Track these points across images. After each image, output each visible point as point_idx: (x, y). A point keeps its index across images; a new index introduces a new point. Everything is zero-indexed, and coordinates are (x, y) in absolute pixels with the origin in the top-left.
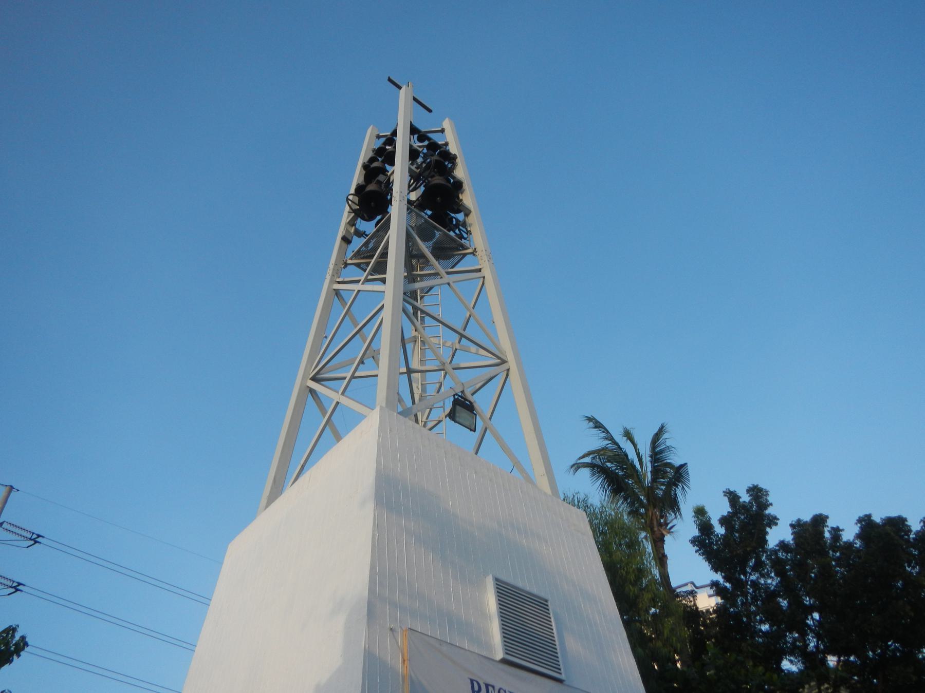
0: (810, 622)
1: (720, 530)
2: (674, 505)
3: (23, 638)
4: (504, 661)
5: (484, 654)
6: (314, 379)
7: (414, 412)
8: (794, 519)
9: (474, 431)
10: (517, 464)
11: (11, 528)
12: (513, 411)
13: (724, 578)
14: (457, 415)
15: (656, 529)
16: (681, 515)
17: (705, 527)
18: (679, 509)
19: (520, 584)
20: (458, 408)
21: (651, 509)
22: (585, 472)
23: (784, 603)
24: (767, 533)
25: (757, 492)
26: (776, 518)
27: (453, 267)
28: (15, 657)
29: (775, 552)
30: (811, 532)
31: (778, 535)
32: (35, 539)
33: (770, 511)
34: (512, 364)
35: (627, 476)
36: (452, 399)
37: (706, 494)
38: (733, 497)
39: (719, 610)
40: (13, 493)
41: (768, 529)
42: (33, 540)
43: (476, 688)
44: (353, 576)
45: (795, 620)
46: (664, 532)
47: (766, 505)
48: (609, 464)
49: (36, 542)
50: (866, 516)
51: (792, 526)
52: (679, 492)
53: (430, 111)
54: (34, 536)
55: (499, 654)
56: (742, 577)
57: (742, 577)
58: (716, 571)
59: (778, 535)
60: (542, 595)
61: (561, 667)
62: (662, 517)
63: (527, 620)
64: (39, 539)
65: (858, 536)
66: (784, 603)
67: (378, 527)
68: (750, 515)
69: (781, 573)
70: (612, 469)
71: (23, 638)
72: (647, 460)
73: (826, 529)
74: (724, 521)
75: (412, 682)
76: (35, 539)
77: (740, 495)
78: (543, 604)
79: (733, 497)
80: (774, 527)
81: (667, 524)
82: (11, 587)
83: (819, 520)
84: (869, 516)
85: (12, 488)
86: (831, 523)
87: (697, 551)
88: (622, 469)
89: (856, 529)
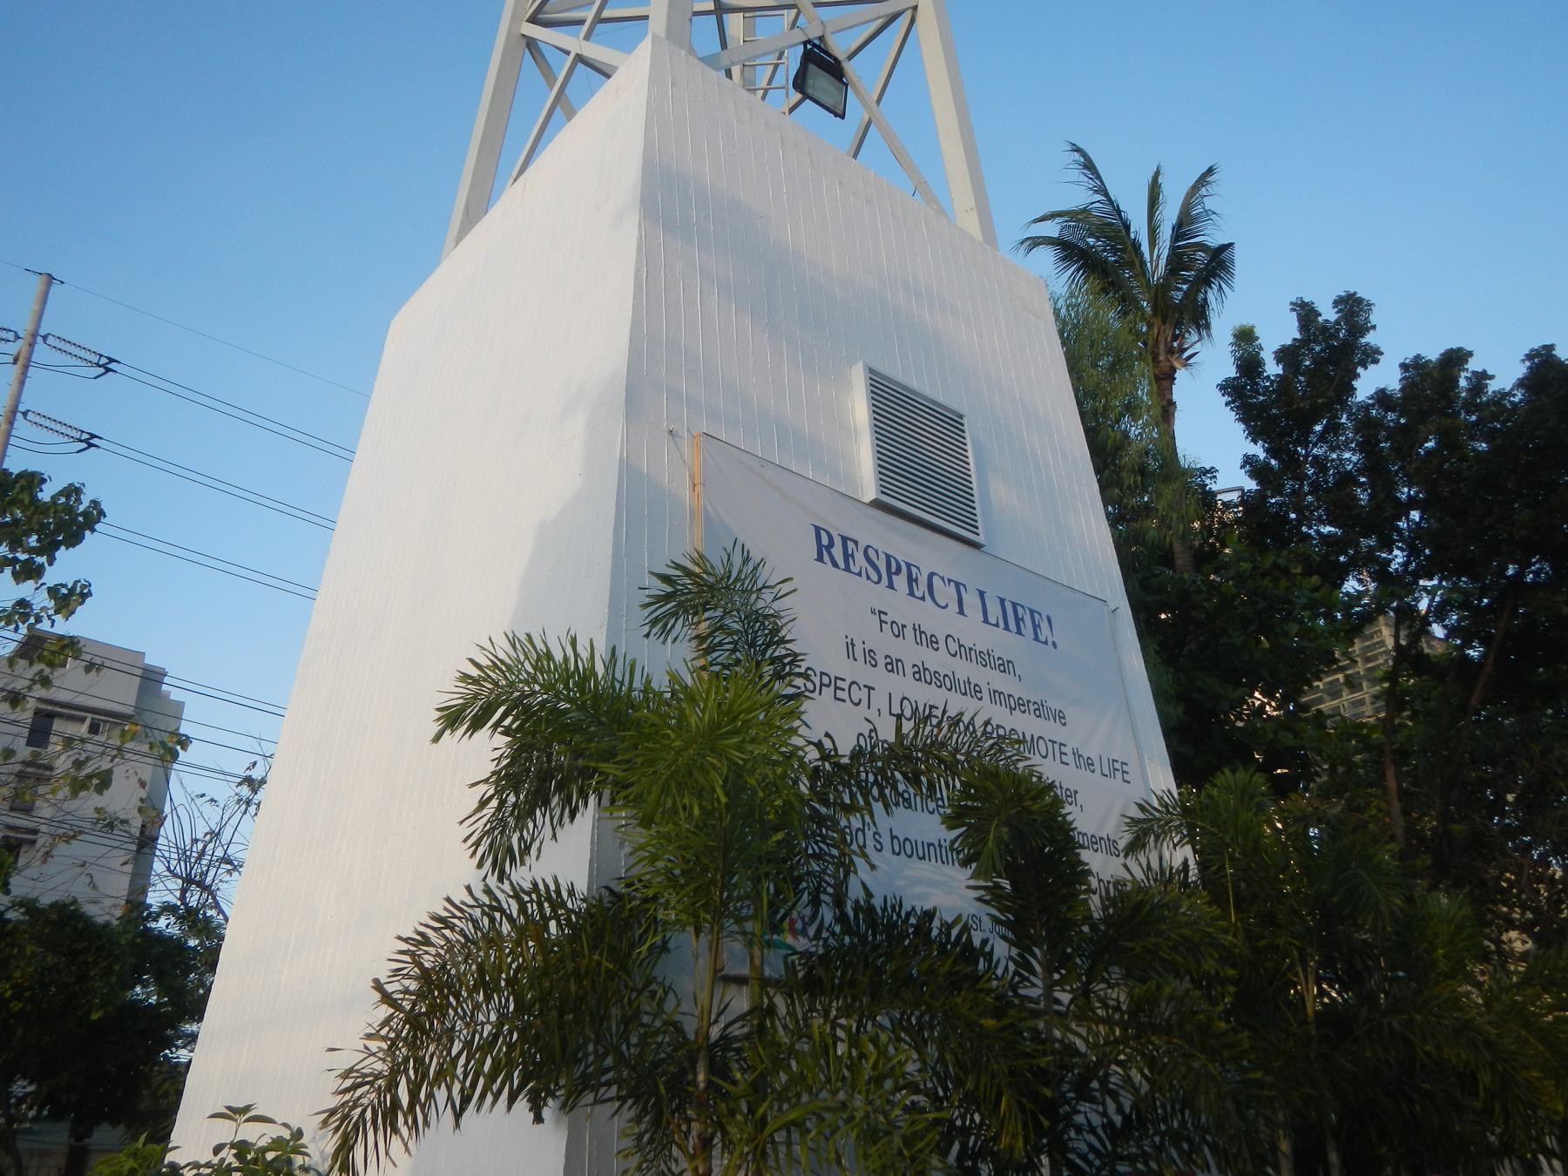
0: (1402, 524)
1: (1273, 369)
2: (1198, 317)
3: (95, 504)
4: (876, 504)
5: (843, 490)
6: (533, 20)
7: (725, 62)
8: (1408, 355)
9: (843, 117)
10: (921, 187)
11: (37, 419)
12: (924, 83)
13: (1267, 451)
14: (810, 82)
15: (1162, 358)
16: (1209, 335)
17: (1249, 365)
18: (1208, 326)
19: (914, 384)
20: (812, 67)
21: (1157, 322)
22: (1046, 257)
23: (1363, 497)
24: (1357, 376)
25: (1353, 308)
26: (1378, 352)
28: (87, 533)
29: (1366, 408)
30: (1435, 380)
31: (1376, 380)
32: (107, 366)
33: (1370, 339)
35: (1123, 264)
36: (801, 49)
37: (1259, 306)
38: (1306, 313)
39: (1246, 499)
40: (55, 288)
41: (1360, 370)
43: (825, 541)
44: (598, 339)
45: (1381, 522)
46: (1176, 365)
47: (1365, 328)
48: (1091, 241)
49: (108, 370)
50: (1545, 347)
51: (1404, 367)
55: (870, 492)
58: (1255, 441)
59: (1376, 380)
60: (954, 406)
61: (979, 524)
62: (1175, 338)
63: (924, 453)
64: (113, 366)
65: (1521, 384)
66: (1363, 497)
67: (646, 252)
68: (1333, 343)
69: (1367, 447)
70: (1095, 249)
71: (95, 504)
72: (1166, 233)
73: (1463, 374)
74: (1283, 355)
75: (707, 517)
76: (107, 366)
77: (1320, 309)
78: (954, 422)
79: (1306, 313)
80: (1372, 367)
82: (80, 440)
83: (1455, 359)
84: (1550, 348)
86: (1473, 365)
87: (1227, 404)
88: (1114, 251)
89: (1521, 370)
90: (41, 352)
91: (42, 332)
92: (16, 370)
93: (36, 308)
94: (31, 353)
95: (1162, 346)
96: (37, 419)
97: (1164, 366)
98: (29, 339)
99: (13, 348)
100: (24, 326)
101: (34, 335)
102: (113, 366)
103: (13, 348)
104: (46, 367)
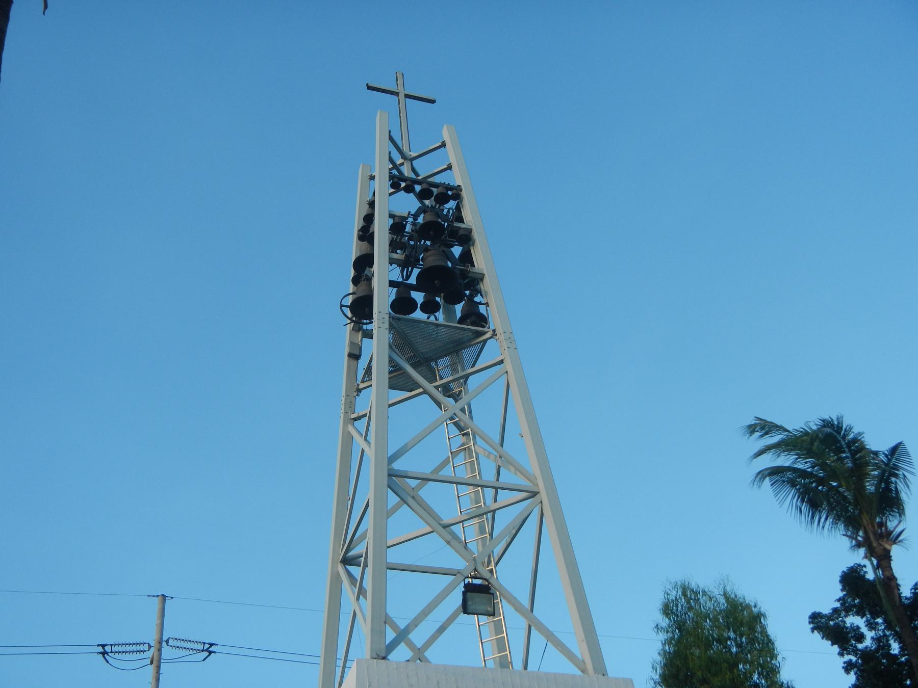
11: (178, 644)
15: (875, 544)
27: (473, 366)
32: (209, 649)
34: (543, 495)
40: (168, 602)
42: (207, 650)
46: (887, 546)
49: (210, 653)
52: (901, 486)
53: (433, 102)
54: (207, 646)
56: (895, 648)
57: (895, 648)
64: (213, 649)
76: (209, 649)
81: (890, 533)
82: (203, 651)
85: (164, 597)
90: (167, 652)
91: (165, 638)
92: (151, 669)
93: (159, 621)
94: (160, 655)
95: (872, 537)
96: (178, 644)
97: (879, 550)
98: (158, 646)
99: (149, 654)
100: (152, 639)
101: (160, 643)
102: (213, 649)
103: (149, 654)
104: (171, 660)
